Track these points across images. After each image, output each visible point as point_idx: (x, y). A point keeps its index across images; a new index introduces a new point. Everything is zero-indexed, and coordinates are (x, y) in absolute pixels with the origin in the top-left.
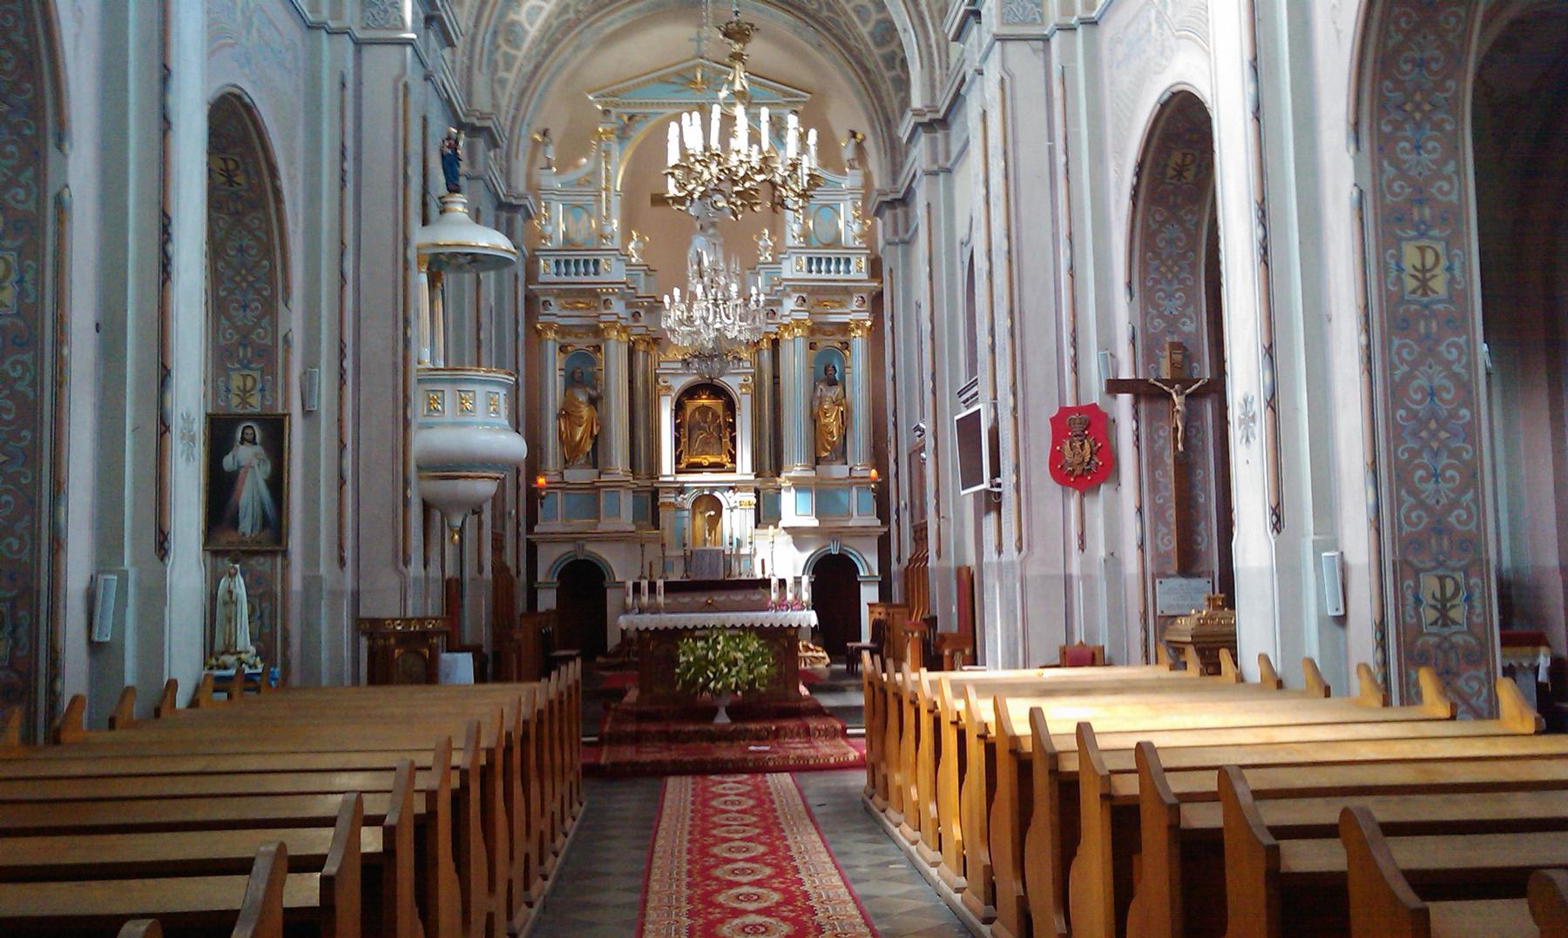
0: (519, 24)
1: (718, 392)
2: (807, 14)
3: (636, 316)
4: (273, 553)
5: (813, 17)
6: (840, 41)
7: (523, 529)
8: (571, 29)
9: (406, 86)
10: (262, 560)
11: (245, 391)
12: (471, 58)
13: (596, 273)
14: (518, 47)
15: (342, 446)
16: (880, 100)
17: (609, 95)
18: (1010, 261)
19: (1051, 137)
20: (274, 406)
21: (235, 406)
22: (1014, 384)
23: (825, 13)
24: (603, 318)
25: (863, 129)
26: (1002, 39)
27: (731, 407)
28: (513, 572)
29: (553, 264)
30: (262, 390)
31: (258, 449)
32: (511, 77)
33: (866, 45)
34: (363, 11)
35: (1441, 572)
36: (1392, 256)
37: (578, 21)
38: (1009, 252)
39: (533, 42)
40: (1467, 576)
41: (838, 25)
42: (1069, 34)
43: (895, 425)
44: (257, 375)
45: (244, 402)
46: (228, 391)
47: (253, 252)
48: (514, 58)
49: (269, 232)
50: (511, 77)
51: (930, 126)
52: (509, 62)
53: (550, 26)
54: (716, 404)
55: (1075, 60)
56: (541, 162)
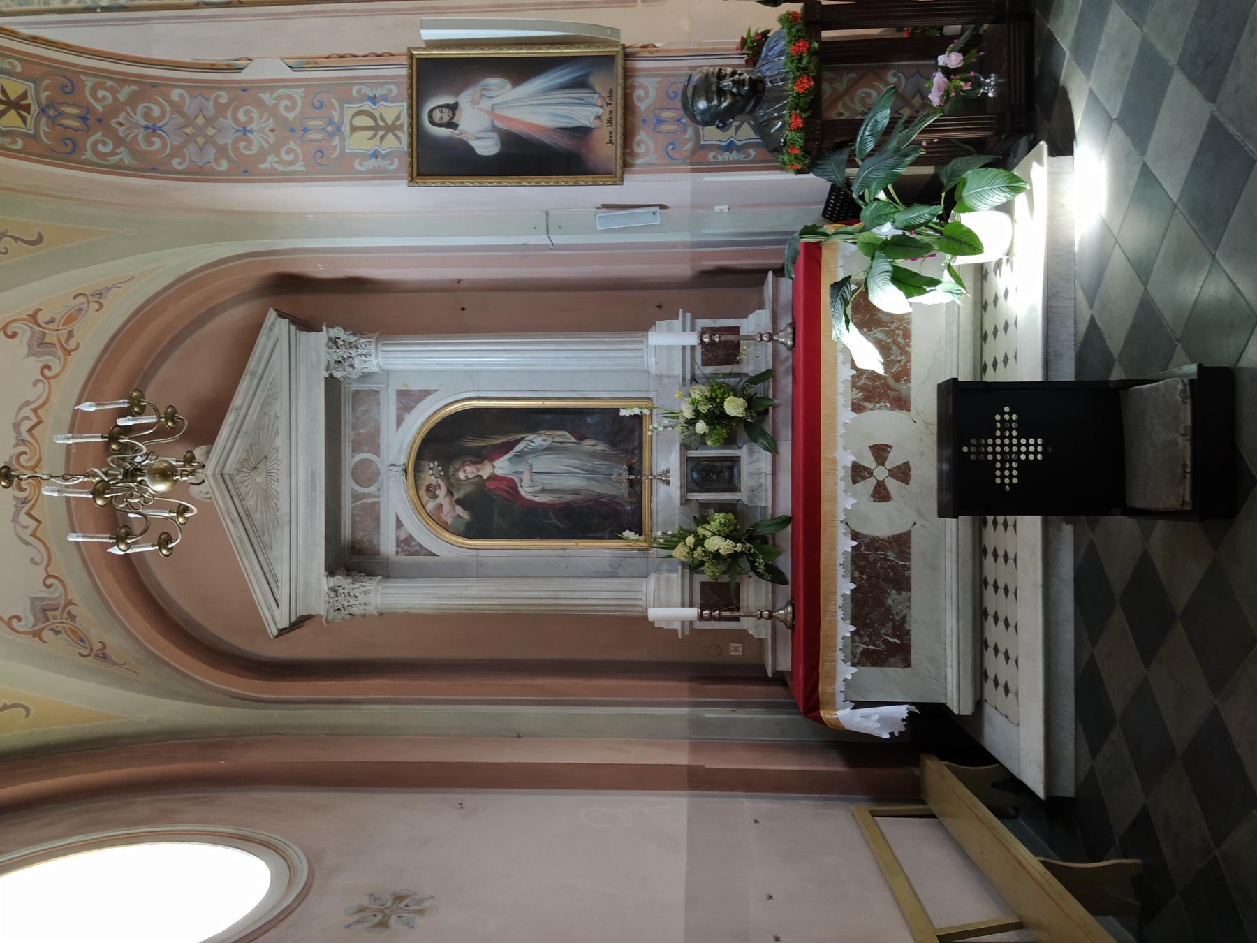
4: (628, 74)
10: (639, 92)
11: (375, 128)
21: (399, 143)
30: (374, 100)
31: (464, 99)
35: (346, 128)
36: (14, 67)
40: (350, 100)
44: (351, 109)
45: (392, 128)
46: (375, 155)
47: (156, 112)
49: (124, 80)
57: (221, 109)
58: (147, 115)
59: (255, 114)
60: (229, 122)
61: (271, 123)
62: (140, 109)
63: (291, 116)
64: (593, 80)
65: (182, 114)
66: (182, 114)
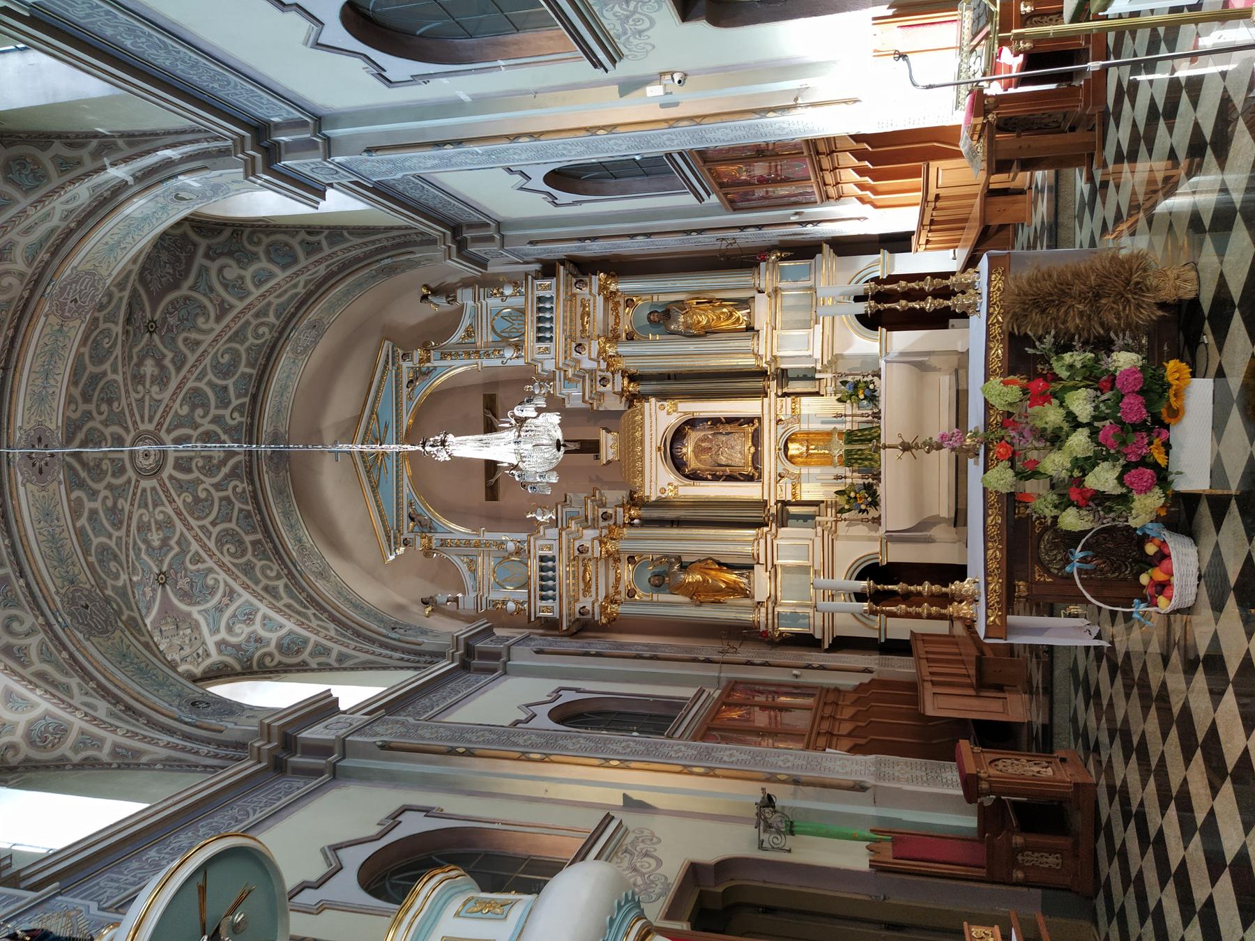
0: (31, 723)
1: (679, 435)
2: (278, 339)
3: (606, 517)
5: (281, 334)
6: (302, 303)
8: (297, 584)
12: (208, 742)
13: (553, 559)
14: (306, 641)
16: (357, 259)
17: (389, 540)
27: (692, 423)
28: (866, 678)
29: (544, 603)
32: (336, 648)
33: (296, 274)
37: (290, 575)
39: (301, 625)
48: (317, 645)
50: (336, 648)
51: (461, 245)
52: (87, 741)
53: (289, 606)
54: (693, 437)
55: (526, 235)
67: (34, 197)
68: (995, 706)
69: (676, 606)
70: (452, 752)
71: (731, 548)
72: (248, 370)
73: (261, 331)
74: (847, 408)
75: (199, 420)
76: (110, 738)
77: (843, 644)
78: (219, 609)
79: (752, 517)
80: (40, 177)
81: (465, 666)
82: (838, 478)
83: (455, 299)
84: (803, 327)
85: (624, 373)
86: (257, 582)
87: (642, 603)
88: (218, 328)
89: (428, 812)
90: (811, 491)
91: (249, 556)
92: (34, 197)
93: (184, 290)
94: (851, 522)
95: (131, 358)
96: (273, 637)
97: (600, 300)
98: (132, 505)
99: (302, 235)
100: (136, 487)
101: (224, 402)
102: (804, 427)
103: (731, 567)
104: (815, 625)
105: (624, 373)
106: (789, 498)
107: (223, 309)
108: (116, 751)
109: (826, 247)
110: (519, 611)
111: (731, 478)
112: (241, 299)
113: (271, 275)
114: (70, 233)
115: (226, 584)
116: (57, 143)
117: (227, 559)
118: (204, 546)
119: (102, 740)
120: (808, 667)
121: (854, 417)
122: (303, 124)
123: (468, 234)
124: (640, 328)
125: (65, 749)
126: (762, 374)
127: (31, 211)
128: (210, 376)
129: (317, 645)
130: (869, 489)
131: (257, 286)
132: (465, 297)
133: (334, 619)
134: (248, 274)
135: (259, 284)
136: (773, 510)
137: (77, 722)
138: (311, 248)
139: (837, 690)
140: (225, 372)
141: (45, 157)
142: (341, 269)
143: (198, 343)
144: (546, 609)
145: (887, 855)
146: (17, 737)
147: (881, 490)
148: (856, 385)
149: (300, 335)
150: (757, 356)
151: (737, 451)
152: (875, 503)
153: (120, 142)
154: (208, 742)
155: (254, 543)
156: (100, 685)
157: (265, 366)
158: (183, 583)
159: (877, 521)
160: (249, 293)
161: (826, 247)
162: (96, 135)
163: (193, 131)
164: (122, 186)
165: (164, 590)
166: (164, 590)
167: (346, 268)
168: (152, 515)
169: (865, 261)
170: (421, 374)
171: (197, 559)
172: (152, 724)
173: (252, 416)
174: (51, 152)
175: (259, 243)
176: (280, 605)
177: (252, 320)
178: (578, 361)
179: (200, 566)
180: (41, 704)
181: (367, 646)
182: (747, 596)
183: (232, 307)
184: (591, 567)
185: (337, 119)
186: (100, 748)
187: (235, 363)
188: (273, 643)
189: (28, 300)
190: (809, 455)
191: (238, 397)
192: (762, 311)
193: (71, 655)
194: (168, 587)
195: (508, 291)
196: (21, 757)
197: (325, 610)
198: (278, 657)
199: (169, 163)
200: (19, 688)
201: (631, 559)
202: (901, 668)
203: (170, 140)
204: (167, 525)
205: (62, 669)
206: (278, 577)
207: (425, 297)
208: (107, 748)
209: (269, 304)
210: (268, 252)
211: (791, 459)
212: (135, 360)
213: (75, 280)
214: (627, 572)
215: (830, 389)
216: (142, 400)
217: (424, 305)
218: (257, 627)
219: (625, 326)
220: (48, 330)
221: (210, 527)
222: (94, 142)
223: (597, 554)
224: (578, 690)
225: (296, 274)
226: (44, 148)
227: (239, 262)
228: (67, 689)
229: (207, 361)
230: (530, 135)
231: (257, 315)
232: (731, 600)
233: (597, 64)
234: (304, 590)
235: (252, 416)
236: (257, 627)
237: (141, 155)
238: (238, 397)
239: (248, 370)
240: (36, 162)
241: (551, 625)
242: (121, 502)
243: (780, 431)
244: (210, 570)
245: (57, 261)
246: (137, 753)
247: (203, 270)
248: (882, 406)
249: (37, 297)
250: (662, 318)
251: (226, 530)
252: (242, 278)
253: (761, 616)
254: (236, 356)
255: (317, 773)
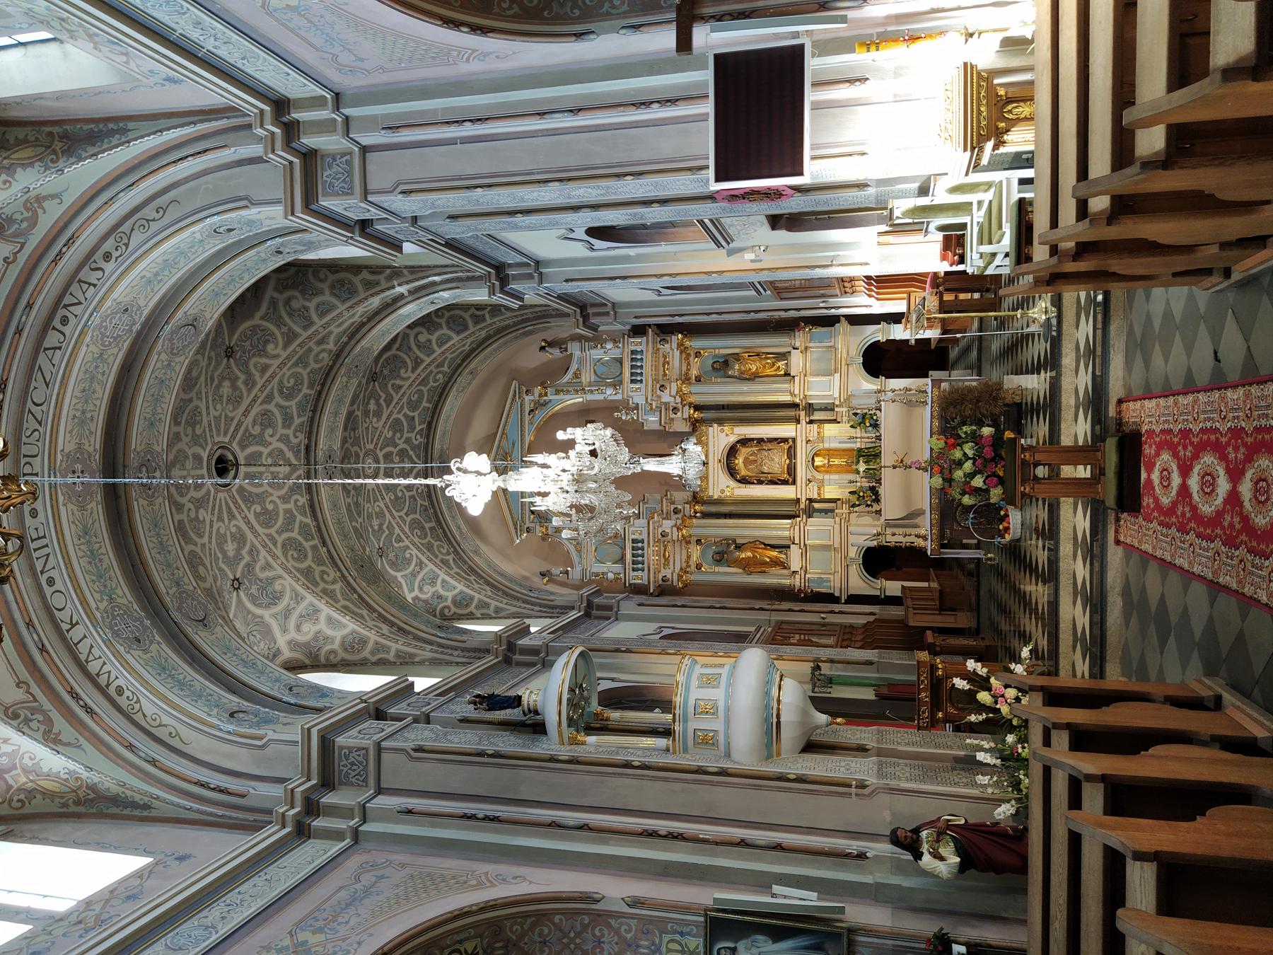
0: (344, 638)
1: (732, 452)
2: (448, 382)
3: (676, 511)
4: (851, 943)
5: (450, 378)
7: (836, 607)
8: (461, 558)
9: (416, 750)
12: (456, 649)
13: (642, 541)
14: (472, 598)
15: (743, 843)
16: (508, 327)
18: (569, 179)
19: (451, 142)
20: (695, 923)
22: (689, 169)
23: (445, 368)
24: (675, 538)
25: (536, 340)
26: (366, 192)
27: (745, 442)
28: (871, 618)
30: (682, 934)
32: (493, 603)
33: (466, 338)
34: (352, 784)
37: (456, 551)
38: (560, 180)
39: (468, 587)
41: (453, 359)
42: (353, 125)
43: (757, 312)
44: (666, 938)
47: (546, 931)
49: (526, 915)
51: (504, 280)
52: (379, 648)
53: (458, 574)
54: (744, 452)
56: (562, 577)
57: (585, 927)
58: (540, 935)
59: (606, 932)
60: (589, 936)
61: (616, 939)
62: (537, 931)
63: (629, 936)
64: (826, 946)
65: (561, 931)
66: (561, 931)
67: (348, 305)
68: (952, 619)
69: (731, 575)
70: (618, 650)
71: (774, 533)
72: (309, 391)
73: (321, 357)
74: (858, 432)
75: (268, 438)
76: (394, 647)
77: (854, 599)
78: (414, 575)
79: (788, 510)
80: (352, 292)
81: (587, 615)
82: (851, 482)
83: (566, 350)
84: (824, 373)
85: (690, 405)
86: (436, 557)
87: (706, 572)
88: (413, 376)
89: (613, 680)
90: (830, 492)
91: (429, 538)
92: (348, 305)
93: (256, 320)
94: (861, 514)
95: (212, 381)
96: (450, 595)
97: (677, 353)
98: (213, 514)
99: (473, 310)
100: (215, 499)
101: (412, 429)
102: (827, 446)
103: (773, 547)
104: (834, 585)
105: (690, 405)
106: (816, 496)
107: (417, 362)
108: (399, 654)
109: (843, 319)
110: (616, 579)
111: (772, 482)
112: (428, 355)
113: (450, 338)
114: (362, 325)
115: (293, 590)
116: (365, 271)
117: (416, 540)
118: (402, 530)
119: (389, 648)
120: (832, 612)
121: (862, 438)
122: (528, 265)
123: (512, 272)
124: (705, 373)
125: (366, 653)
126: (795, 406)
127: (345, 313)
128: (406, 410)
129: (480, 601)
130: (873, 490)
131: (440, 347)
132: (574, 349)
133: (488, 583)
134: (434, 338)
135: (322, 315)
136: (802, 506)
137: (372, 637)
138: (478, 320)
139: (851, 626)
140: (413, 406)
141: (356, 280)
142: (496, 333)
143: (400, 387)
144: (639, 578)
145: (885, 691)
146: (336, 646)
147: (881, 491)
148: (864, 416)
149: (462, 380)
150: (792, 394)
151: (776, 462)
152: (877, 500)
153: (405, 271)
154: (456, 649)
155: (432, 529)
156: (380, 615)
157: (438, 402)
158: (391, 556)
159: (879, 512)
160: (434, 352)
161: (843, 319)
162: (389, 267)
163: (453, 266)
164: (402, 296)
165: (238, 595)
166: (238, 595)
167: (499, 333)
168: (228, 528)
169: (871, 329)
170: (539, 405)
171: (399, 540)
172: (416, 638)
173: (428, 437)
174: (361, 277)
175: (442, 316)
176: (452, 572)
177: (314, 347)
178: (659, 397)
179: (401, 544)
180: (350, 626)
181: (514, 602)
182: (785, 568)
183: (422, 361)
184: (670, 547)
185: (548, 263)
186: (388, 653)
187: (420, 401)
188: (450, 600)
189: (332, 367)
190: (830, 466)
191: (299, 416)
192: (797, 361)
193: (360, 596)
194: (241, 593)
195: (609, 346)
196: (339, 658)
197: (482, 577)
198: (453, 609)
199: (434, 284)
200: (335, 615)
201: (698, 542)
202: (895, 612)
203: (437, 270)
204: (380, 515)
205: (358, 605)
206: (334, 582)
207: (542, 348)
208: (392, 653)
209: (331, 333)
210: (448, 323)
211: (816, 468)
212: (216, 382)
213: (360, 354)
214: (696, 552)
215: (845, 419)
216: (367, 428)
217: (542, 354)
218: (322, 625)
219: (694, 372)
220: (159, 365)
221: (276, 536)
222: (388, 271)
223: (675, 538)
224: (613, 680)
225: (466, 338)
226: (356, 274)
227: (428, 330)
228: (362, 617)
229: (405, 399)
230: (670, 275)
231: (437, 367)
232: (773, 570)
233: (719, 245)
234: (466, 563)
235: (428, 437)
236: (322, 625)
237: (417, 280)
238: (299, 416)
239: (309, 391)
240: (350, 282)
241: (639, 590)
242: (202, 512)
243: (809, 448)
244: (280, 577)
245: (353, 343)
246: (412, 656)
247: (273, 303)
248: (882, 431)
249: (337, 366)
250: (723, 366)
251: (289, 539)
252: (430, 341)
253: (797, 582)
254: (421, 393)
255: (533, 664)
